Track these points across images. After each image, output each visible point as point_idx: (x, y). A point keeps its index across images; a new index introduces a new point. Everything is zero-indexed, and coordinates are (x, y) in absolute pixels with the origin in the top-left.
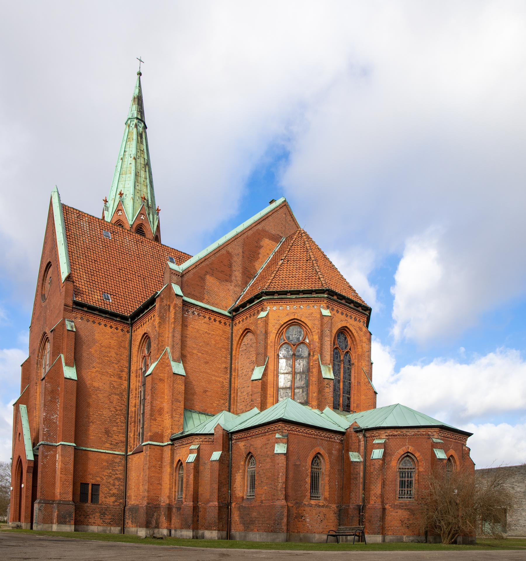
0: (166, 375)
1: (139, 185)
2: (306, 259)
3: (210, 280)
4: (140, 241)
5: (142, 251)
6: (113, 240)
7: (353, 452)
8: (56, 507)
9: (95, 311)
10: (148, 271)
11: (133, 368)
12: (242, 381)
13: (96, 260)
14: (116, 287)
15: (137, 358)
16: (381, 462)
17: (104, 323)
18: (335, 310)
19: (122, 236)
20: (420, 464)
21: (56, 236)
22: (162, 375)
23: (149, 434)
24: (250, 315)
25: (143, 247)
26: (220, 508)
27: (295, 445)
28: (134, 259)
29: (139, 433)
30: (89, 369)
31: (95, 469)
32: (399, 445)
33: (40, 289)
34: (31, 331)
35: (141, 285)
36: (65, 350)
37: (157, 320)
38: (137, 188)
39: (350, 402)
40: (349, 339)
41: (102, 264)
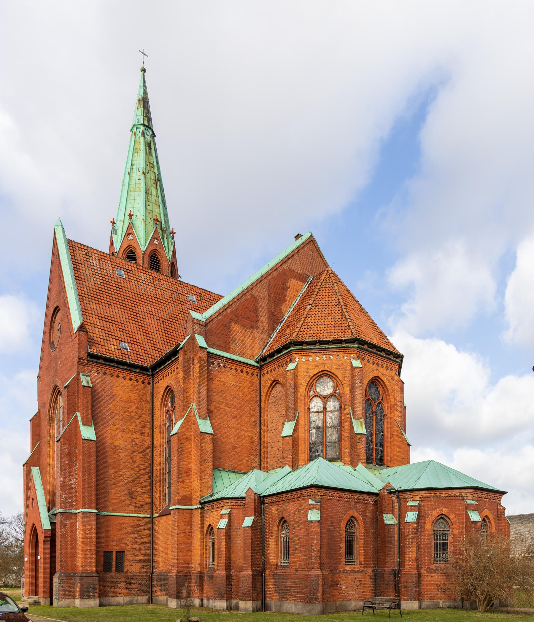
1: (151, 204)
2: (334, 304)
3: (235, 328)
4: (157, 279)
5: (159, 290)
6: (127, 279)
7: (387, 514)
9: (112, 363)
10: (167, 313)
11: (156, 423)
12: (272, 435)
13: (110, 304)
14: (134, 334)
15: (161, 412)
16: (415, 525)
17: (123, 376)
18: (366, 360)
20: (455, 526)
21: (63, 278)
22: (188, 434)
23: (177, 498)
26: (254, 576)
27: (328, 510)
28: (151, 300)
29: (166, 494)
32: (432, 507)
35: (160, 330)
36: (81, 408)
37: (181, 376)
38: (148, 207)
40: (381, 389)
41: (116, 308)
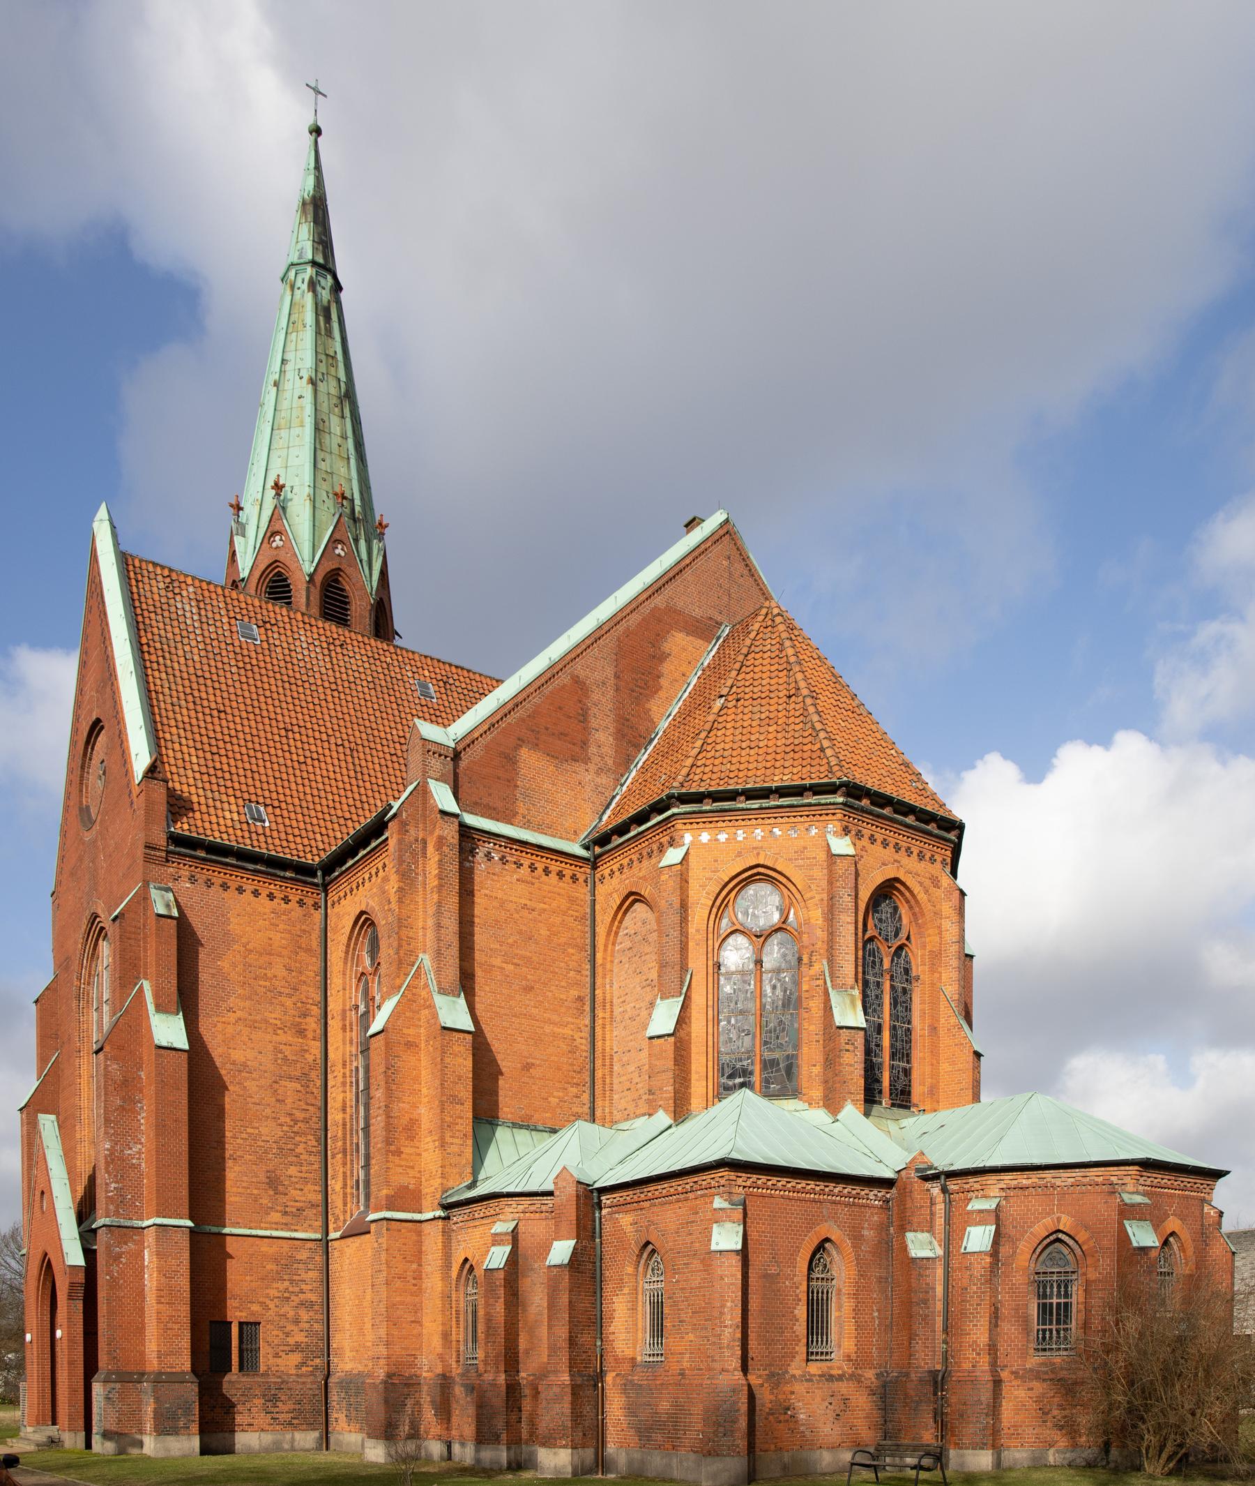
0: (422, 1030)
1: (328, 457)
2: (785, 692)
3: (531, 761)
4: (337, 643)
5: (343, 670)
6: (265, 645)
8: (150, 1390)
10: (362, 728)
12: (624, 1033)
18: (866, 837)
19: (289, 633)
22: (411, 1031)
24: (640, 854)
25: (346, 659)
26: (576, 1390)
27: (763, 1224)
28: (322, 697)
29: (358, 1181)
30: (218, 1016)
31: (246, 1281)
33: (75, 792)
34: (57, 907)
36: (152, 970)
38: (322, 465)
39: (910, 1081)
40: (904, 911)
41: (238, 720)
